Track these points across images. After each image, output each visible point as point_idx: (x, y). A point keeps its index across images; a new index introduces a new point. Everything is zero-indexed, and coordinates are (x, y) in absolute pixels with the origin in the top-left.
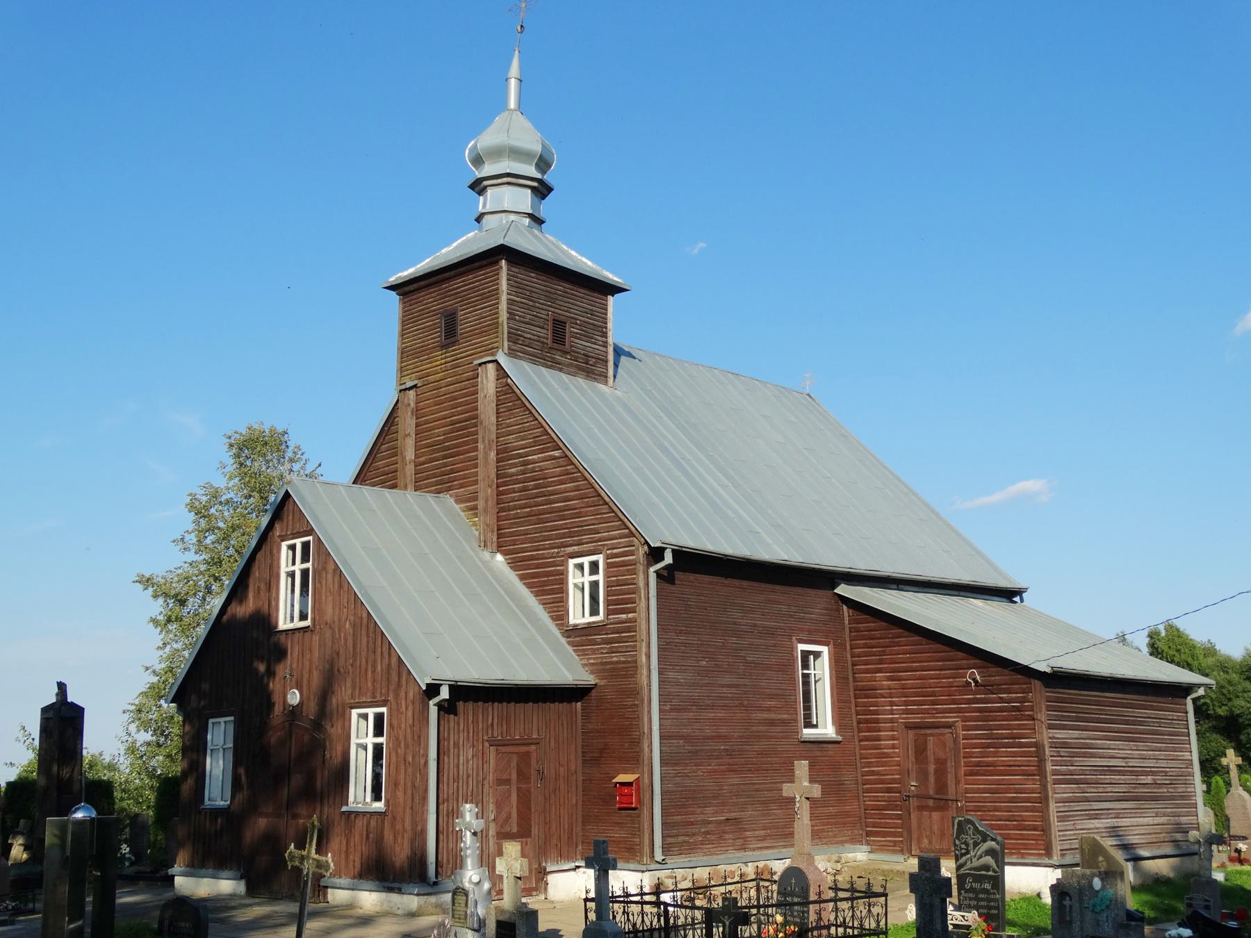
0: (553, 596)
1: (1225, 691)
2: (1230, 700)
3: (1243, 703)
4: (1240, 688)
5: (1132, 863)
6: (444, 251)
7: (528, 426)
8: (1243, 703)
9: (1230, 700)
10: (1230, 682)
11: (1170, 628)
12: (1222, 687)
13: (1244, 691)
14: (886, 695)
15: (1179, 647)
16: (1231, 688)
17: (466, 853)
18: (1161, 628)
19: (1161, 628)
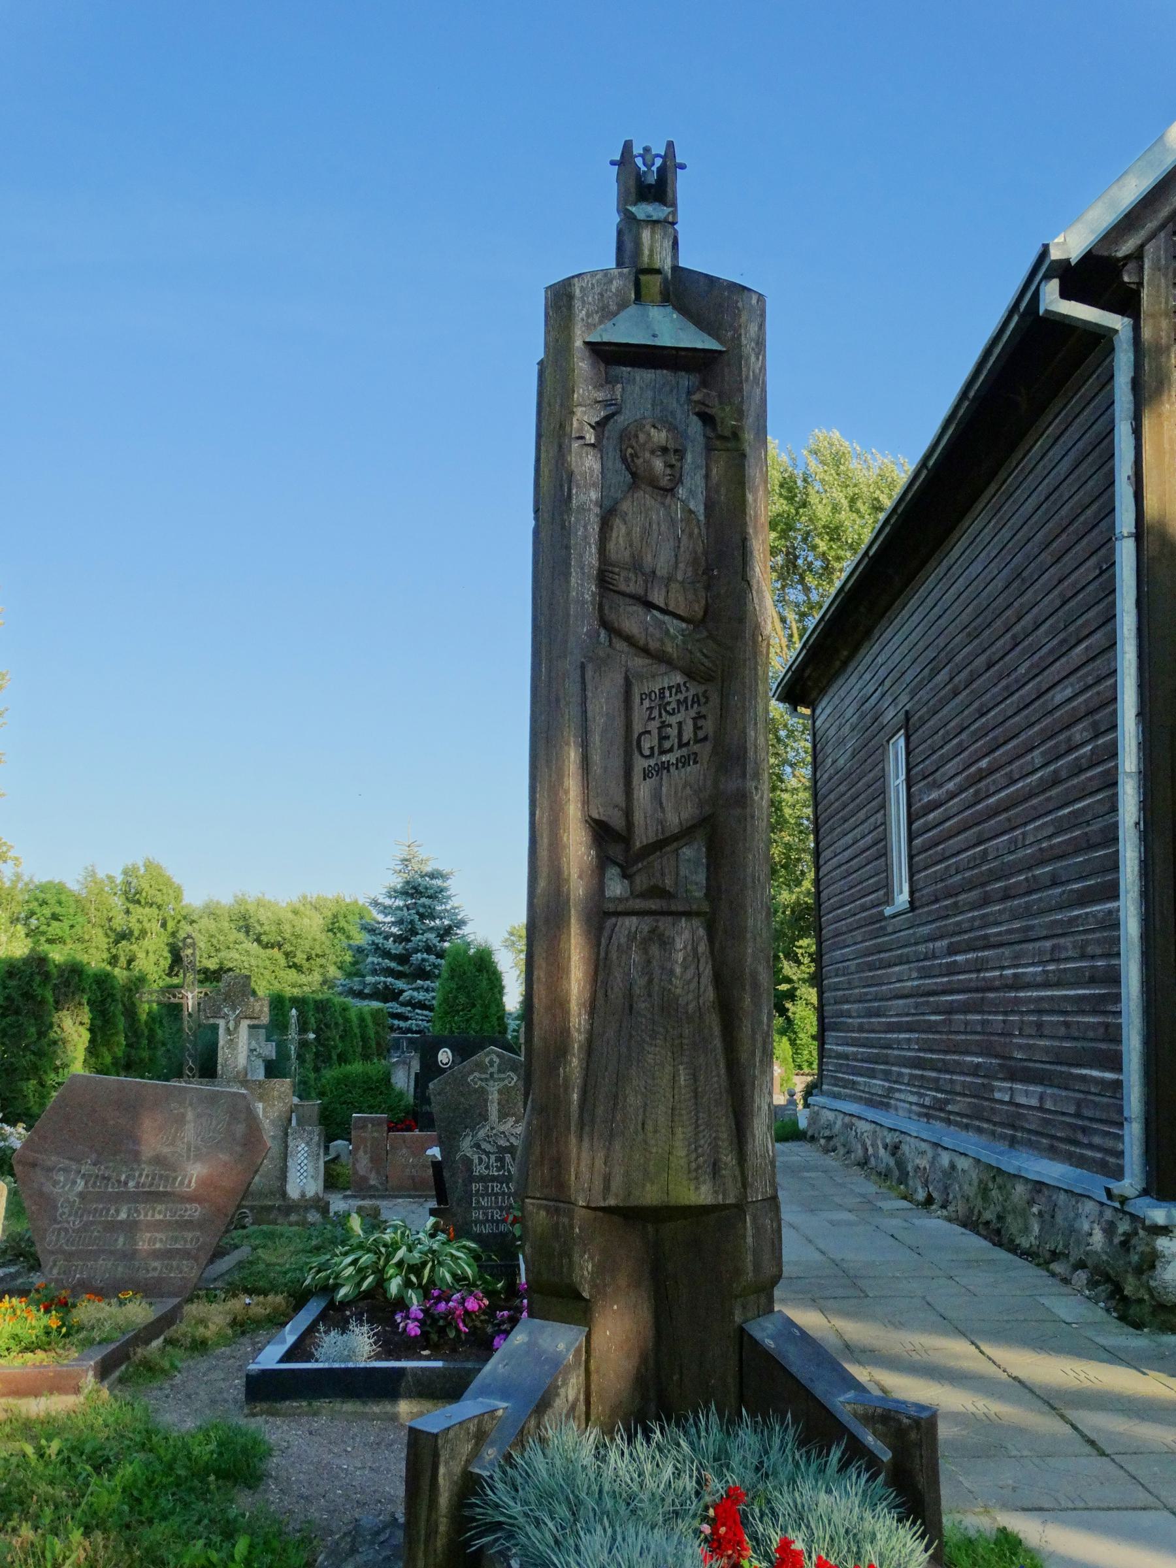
0: (1037, 823)
1: (215, 942)
2: (218, 950)
3: (237, 956)
4: (231, 938)
5: (650, 599)
6: (1078, 833)
7: (1041, 803)
8: (237, 956)
9: (218, 950)
10: (221, 931)
11: (148, 865)
12: (212, 936)
13: (236, 943)
14: (974, 1048)
15: (161, 887)
16: (222, 938)
17: (141, 997)
18: (140, 864)
19: (140, 864)
